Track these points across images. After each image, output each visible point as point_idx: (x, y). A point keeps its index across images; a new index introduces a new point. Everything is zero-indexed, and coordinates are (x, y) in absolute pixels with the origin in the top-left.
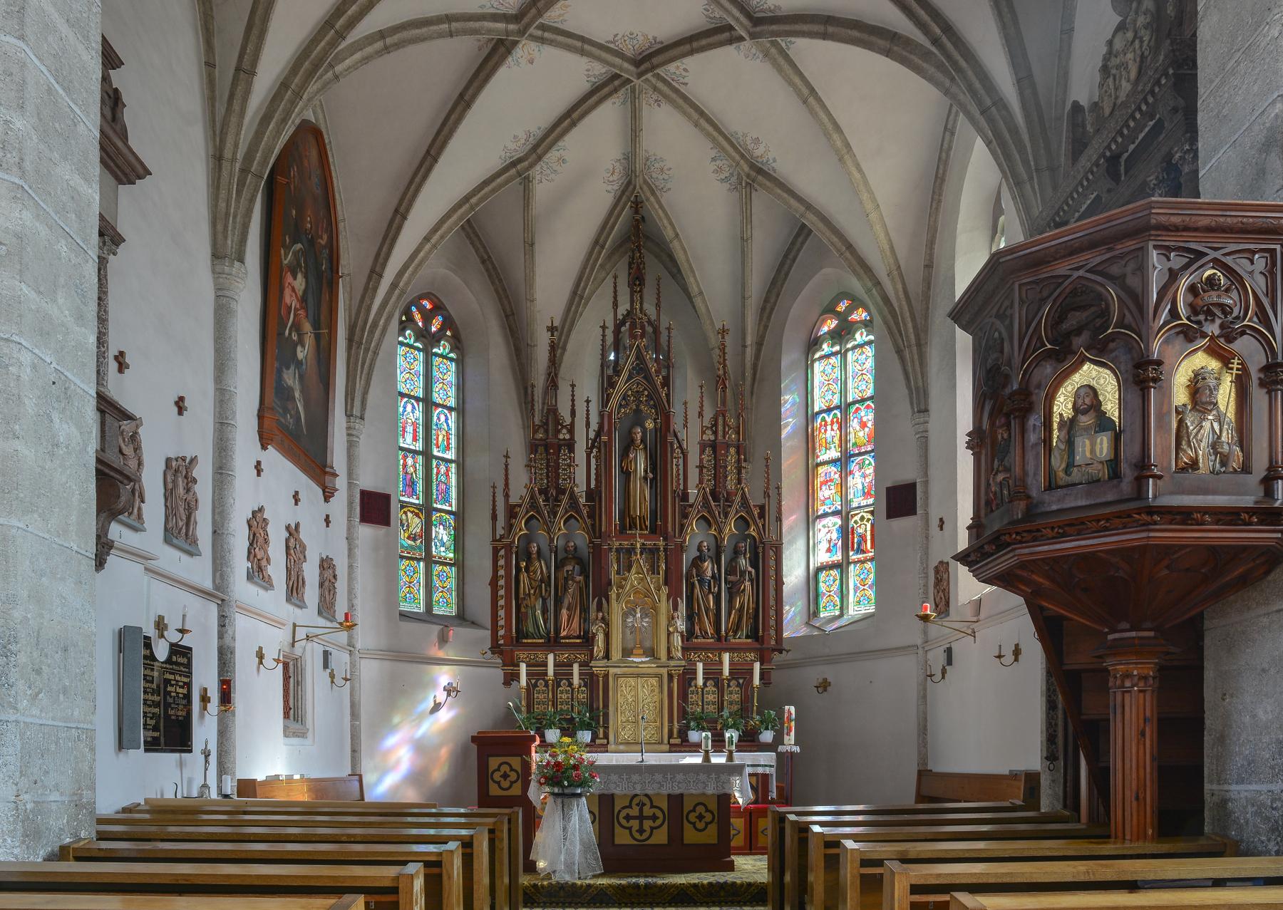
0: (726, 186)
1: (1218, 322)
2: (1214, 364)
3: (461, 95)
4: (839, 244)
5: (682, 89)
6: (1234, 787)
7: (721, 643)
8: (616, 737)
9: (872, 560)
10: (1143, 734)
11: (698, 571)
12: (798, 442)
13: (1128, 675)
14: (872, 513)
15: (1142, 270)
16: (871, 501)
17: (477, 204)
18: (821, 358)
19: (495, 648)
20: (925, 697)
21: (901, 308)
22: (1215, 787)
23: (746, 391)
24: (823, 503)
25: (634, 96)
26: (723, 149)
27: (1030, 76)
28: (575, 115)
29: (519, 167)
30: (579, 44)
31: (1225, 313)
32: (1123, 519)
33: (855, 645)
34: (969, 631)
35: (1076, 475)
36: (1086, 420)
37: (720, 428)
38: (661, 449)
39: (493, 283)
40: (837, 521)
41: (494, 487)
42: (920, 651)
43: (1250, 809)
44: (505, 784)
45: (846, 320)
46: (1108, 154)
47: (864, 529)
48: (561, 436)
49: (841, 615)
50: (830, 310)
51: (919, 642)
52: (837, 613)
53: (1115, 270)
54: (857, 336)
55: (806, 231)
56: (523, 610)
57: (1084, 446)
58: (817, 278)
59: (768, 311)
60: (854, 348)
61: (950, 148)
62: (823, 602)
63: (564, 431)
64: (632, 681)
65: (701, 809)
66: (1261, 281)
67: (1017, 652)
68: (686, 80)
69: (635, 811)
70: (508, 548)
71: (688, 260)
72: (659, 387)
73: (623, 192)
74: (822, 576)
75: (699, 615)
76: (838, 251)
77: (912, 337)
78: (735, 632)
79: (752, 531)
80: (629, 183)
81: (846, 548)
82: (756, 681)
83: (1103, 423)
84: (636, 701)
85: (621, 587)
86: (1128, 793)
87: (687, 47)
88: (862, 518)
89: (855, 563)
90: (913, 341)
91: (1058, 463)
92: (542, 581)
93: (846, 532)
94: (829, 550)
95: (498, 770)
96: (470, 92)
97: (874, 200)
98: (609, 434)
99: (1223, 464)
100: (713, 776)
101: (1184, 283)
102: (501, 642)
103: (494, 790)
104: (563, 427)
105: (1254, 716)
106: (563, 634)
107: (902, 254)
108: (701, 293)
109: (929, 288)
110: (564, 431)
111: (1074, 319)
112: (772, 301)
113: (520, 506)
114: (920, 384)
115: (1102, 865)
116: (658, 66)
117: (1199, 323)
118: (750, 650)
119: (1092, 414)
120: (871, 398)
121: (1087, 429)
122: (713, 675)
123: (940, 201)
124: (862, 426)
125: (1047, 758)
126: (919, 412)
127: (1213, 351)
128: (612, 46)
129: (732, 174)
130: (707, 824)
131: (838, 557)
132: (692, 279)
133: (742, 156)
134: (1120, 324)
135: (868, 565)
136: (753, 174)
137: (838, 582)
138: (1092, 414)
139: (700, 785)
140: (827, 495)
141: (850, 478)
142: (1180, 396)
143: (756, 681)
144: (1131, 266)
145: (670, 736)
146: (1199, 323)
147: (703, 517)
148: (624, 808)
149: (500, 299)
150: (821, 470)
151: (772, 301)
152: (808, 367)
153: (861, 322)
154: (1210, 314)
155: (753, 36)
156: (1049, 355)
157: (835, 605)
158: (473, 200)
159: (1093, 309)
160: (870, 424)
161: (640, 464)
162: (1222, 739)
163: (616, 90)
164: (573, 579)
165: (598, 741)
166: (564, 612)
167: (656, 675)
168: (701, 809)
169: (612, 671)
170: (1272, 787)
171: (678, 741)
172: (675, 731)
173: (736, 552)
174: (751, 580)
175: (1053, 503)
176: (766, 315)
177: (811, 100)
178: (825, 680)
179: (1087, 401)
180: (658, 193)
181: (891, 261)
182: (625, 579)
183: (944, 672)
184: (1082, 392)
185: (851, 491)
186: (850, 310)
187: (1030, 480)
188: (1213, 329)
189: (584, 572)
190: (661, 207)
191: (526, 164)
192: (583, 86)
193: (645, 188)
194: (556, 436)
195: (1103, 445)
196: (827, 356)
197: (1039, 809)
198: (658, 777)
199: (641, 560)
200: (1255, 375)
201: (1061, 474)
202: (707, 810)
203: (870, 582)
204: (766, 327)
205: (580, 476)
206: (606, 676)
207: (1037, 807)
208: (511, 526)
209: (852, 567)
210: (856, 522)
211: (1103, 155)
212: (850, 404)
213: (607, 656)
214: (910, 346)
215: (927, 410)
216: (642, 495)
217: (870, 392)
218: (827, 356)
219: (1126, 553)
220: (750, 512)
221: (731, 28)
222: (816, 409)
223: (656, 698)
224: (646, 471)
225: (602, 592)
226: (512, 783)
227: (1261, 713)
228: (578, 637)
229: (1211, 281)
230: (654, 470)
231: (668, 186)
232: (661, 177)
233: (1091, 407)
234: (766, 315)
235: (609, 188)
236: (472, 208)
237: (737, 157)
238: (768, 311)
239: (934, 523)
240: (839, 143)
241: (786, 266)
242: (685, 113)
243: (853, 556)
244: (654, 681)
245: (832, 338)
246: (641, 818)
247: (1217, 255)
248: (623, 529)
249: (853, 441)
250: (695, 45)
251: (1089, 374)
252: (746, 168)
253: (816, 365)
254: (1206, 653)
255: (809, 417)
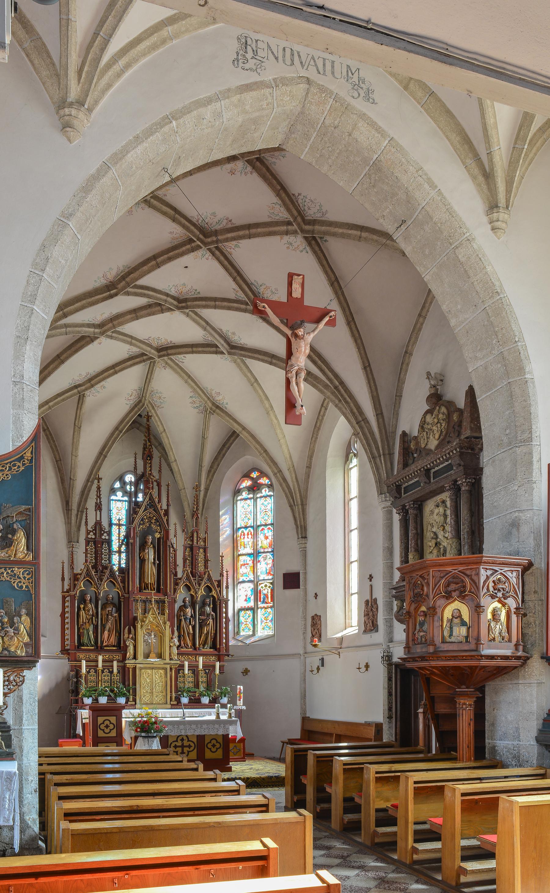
0: (197, 410)
1: (501, 593)
2: (499, 605)
3: (58, 356)
4: (260, 449)
5: (180, 364)
6: (498, 742)
7: (196, 651)
8: (141, 701)
9: (271, 607)
10: (470, 724)
11: (184, 613)
12: (229, 542)
13: (465, 704)
14: (271, 583)
15: (478, 574)
16: (270, 577)
17: (53, 406)
18: (241, 500)
19: (64, 651)
20: (305, 680)
21: (294, 486)
22: (490, 741)
23: (201, 515)
24: (242, 575)
25: (152, 365)
26: (199, 394)
27: (382, 413)
28: (117, 369)
29: (79, 389)
30: (130, 340)
31: (504, 590)
32: (472, 657)
33: (264, 652)
34: (337, 652)
35: (453, 639)
36: (456, 621)
37: (195, 538)
38: (162, 547)
39: (49, 442)
40: (251, 586)
41: (63, 563)
42: (302, 657)
43: (505, 750)
44: (107, 731)
45: (257, 483)
46: (426, 468)
47: (266, 591)
48: (103, 537)
49: (254, 635)
50: (247, 476)
51: (302, 652)
52: (251, 633)
53: (468, 572)
54: (263, 491)
55: (236, 435)
56: (81, 631)
57: (456, 630)
58: (242, 460)
59: (212, 472)
60: (261, 497)
61: (324, 415)
62: (242, 627)
63: (105, 534)
64: (149, 671)
65: (214, 742)
66: (515, 580)
67: (367, 666)
68: (183, 361)
69: (179, 743)
70: (73, 598)
71: (169, 443)
72: (163, 516)
73: (136, 406)
74: (242, 613)
75: (183, 636)
76: (259, 452)
77: (299, 500)
78: (204, 646)
79: (214, 593)
80: (140, 401)
81: (256, 600)
82: (217, 671)
83: (463, 623)
84: (152, 682)
85: (143, 621)
86: (464, 745)
87: (190, 349)
88: (266, 586)
89: (262, 608)
90: (300, 503)
91: (446, 634)
92: (93, 615)
93: (256, 593)
94: (246, 600)
95: (103, 723)
96: (65, 355)
97: (283, 433)
98: (134, 538)
99: (503, 639)
100: (222, 725)
101: (491, 579)
102: (68, 647)
103: (101, 734)
104: (105, 532)
105: (506, 718)
106: (105, 644)
107: (295, 459)
108: (176, 460)
109: (309, 478)
110: (105, 534)
111: (453, 587)
112: (215, 467)
113: (81, 574)
114: (303, 524)
115: (471, 773)
116: (171, 354)
117: (496, 593)
118: (212, 655)
119: (459, 619)
120: (272, 524)
121: (457, 624)
122: (194, 669)
123: (317, 438)
124: (265, 539)
125: (388, 718)
126: (302, 538)
127: (500, 601)
128: (146, 341)
129: (201, 406)
130: (217, 749)
131: (251, 604)
132: (171, 453)
133: (209, 398)
134: (470, 592)
135: (269, 610)
136: (214, 408)
137: (251, 617)
138: (459, 619)
139: (215, 730)
140: (245, 572)
141: (258, 564)
142: (490, 616)
143: (217, 671)
144: (474, 573)
145: (171, 700)
146: (496, 593)
147: (186, 585)
148: (174, 742)
149: (53, 452)
150: (241, 558)
151: (215, 467)
152: (234, 503)
153: (265, 484)
154: (499, 590)
155: (229, 353)
156: (444, 596)
157: (249, 629)
158: (51, 404)
159: (460, 585)
160: (270, 538)
161: (150, 554)
162: (493, 724)
163: (144, 361)
164: (112, 615)
165: (129, 703)
166: (106, 632)
167: (163, 669)
168: (214, 742)
169: (138, 666)
170: (514, 743)
171: (175, 703)
172: (173, 698)
173: (204, 604)
174: (213, 619)
175: (445, 647)
176: (211, 475)
177: (255, 384)
178: (246, 669)
179: (457, 614)
180: (156, 408)
181: (290, 463)
182: (146, 617)
183: (318, 669)
184: (456, 611)
185: (259, 571)
186: (259, 478)
187: (435, 639)
188: (500, 595)
189: (119, 610)
190: (157, 415)
191: (83, 387)
192: (126, 356)
193: (149, 405)
194: (101, 537)
195: (463, 631)
196: (245, 499)
197: (382, 740)
198: (194, 726)
199: (154, 606)
200: (513, 610)
201: (447, 638)
202: (217, 742)
203: (270, 618)
204: (211, 481)
205: (118, 561)
206: (134, 669)
207: (381, 739)
208: (75, 585)
209: (259, 610)
210: (262, 587)
211: (423, 467)
212: (259, 526)
213: (135, 657)
214: (298, 505)
215: (306, 537)
216: (151, 570)
217: (269, 522)
218: (245, 499)
219: (470, 667)
220: (212, 584)
221: (217, 346)
222: (238, 526)
223: (163, 680)
224: (154, 559)
225: (133, 623)
226: (111, 730)
227: (509, 717)
228: (114, 646)
229: (499, 579)
230: (159, 559)
231: (162, 406)
232: (158, 401)
233: (458, 617)
234: (211, 475)
235: (128, 402)
236: (50, 408)
237: (206, 399)
238: (212, 472)
239: (311, 596)
240: (267, 405)
241: (224, 451)
242: (181, 376)
243: (260, 605)
244: (162, 671)
245: (249, 491)
246: (183, 746)
247: (502, 571)
248: (140, 590)
249: (260, 545)
250: (194, 349)
251: (456, 605)
252: (210, 405)
253: (239, 502)
254: (486, 693)
255: (235, 530)
